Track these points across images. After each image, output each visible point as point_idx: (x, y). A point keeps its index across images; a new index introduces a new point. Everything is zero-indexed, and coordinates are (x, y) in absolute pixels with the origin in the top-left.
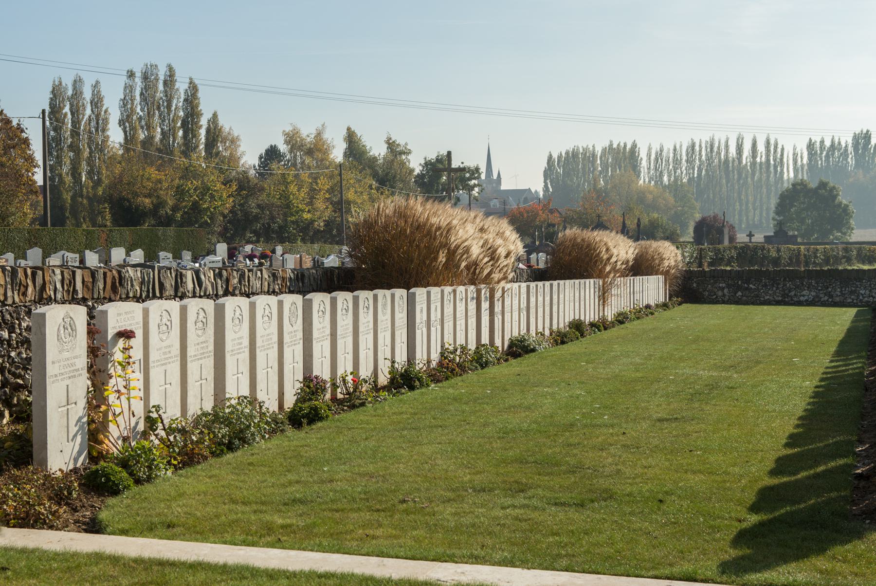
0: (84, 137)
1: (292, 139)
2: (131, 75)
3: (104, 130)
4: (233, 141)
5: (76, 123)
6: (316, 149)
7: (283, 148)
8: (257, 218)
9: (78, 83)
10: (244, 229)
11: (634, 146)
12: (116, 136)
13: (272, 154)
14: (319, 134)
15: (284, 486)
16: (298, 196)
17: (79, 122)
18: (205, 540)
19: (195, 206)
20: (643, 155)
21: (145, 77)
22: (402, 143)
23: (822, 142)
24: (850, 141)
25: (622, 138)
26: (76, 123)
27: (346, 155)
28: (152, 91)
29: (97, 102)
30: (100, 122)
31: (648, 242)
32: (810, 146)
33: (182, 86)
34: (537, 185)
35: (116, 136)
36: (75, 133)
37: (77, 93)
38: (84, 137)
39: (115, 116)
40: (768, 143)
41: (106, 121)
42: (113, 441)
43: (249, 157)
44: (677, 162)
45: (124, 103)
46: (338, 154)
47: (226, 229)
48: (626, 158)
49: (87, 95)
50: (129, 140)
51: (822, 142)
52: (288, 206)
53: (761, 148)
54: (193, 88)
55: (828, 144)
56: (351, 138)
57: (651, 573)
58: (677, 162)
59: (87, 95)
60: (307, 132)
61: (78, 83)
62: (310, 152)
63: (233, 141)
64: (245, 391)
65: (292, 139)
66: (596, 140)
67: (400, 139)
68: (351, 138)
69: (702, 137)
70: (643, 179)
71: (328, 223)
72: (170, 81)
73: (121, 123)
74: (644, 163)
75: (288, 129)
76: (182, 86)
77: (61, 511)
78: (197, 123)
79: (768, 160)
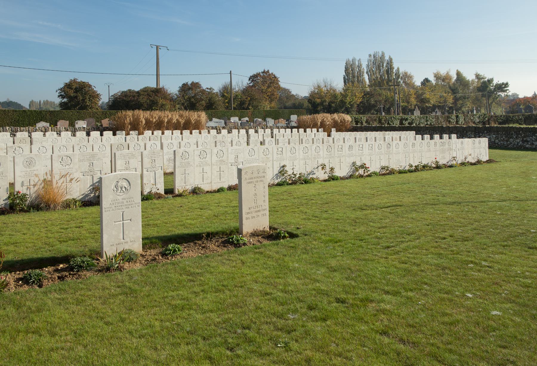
1: (437, 77)
2: (370, 56)
3: (363, 75)
4: (411, 77)
7: (432, 79)
13: (426, 81)
14: (448, 73)
15: (502, 253)
17: (355, 73)
18: (188, 234)
21: (374, 57)
22: (482, 75)
29: (360, 66)
30: (360, 73)
33: (387, 58)
41: (363, 72)
42: (145, 193)
43: (418, 82)
45: (368, 66)
49: (357, 63)
54: (391, 60)
56: (398, 69)
59: (357, 63)
62: (443, 80)
63: (411, 77)
65: (437, 77)
75: (435, 72)
76: (387, 58)
77: (462, 332)
78: (392, 71)
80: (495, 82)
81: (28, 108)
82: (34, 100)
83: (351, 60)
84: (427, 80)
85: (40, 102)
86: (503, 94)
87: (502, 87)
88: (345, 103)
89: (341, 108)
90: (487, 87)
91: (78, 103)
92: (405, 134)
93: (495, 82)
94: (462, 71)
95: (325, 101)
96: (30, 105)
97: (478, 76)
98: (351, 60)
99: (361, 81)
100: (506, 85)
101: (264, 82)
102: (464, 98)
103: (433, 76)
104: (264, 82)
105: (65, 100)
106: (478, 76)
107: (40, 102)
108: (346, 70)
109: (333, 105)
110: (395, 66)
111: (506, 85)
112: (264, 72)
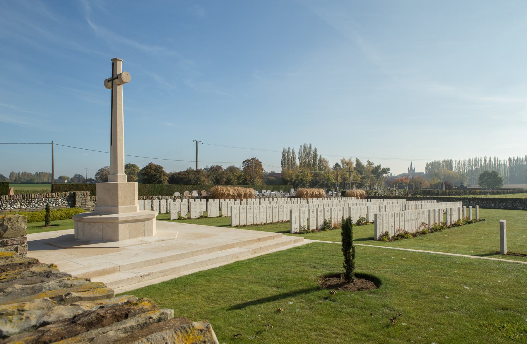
0: (290, 162)
1: (343, 162)
2: (301, 146)
5: (288, 159)
6: (349, 163)
7: (340, 163)
8: (319, 182)
9: (289, 149)
10: (316, 185)
11: (451, 160)
12: (298, 162)
13: (337, 165)
14: (350, 160)
16: (332, 177)
19: (301, 179)
20: (454, 163)
21: (304, 147)
23: (514, 158)
24: (524, 158)
25: (448, 158)
26: (288, 159)
27: (356, 165)
28: (306, 151)
29: (293, 153)
30: (294, 158)
31: (216, 187)
32: (510, 159)
33: (313, 149)
34: (423, 171)
35: (298, 162)
36: (288, 160)
37: (289, 152)
38: (290, 162)
39: (297, 156)
40: (495, 159)
41: (295, 158)
43: (331, 166)
44: (465, 165)
45: (299, 153)
46: (354, 165)
47: (310, 185)
48: (449, 164)
49: (291, 151)
50: (301, 163)
51: (514, 158)
52: (329, 179)
53: (492, 160)
54: (316, 149)
55: (516, 158)
56: (357, 161)
57: (216, 224)
58: (465, 165)
59: (291, 151)
60: (347, 159)
61: (289, 149)
64: (154, 201)
65: (343, 162)
66: (441, 158)
67: (371, 161)
68: (357, 161)
69: (473, 157)
70: (454, 169)
71: (341, 183)
72: (310, 148)
73: (299, 158)
74: (454, 165)
75: (342, 158)
76: (313, 149)
79: (495, 164)
80: (382, 168)
81: (9, 178)
82: (14, 172)
83: (287, 149)
84: (337, 165)
85: (19, 173)
86: (384, 175)
87: (386, 171)
88: (304, 181)
89: (301, 183)
90: (378, 170)
91: (157, 179)
92: (426, 203)
93: (382, 168)
94: (359, 159)
95: (292, 179)
96: (10, 176)
97: (370, 163)
98: (287, 149)
99: (294, 164)
100: (388, 169)
101: (253, 165)
102: (367, 177)
103: (340, 161)
104: (253, 165)
105: (146, 177)
106: (370, 163)
107: (19, 173)
108: (284, 155)
109: (297, 182)
110: (319, 154)
111: (388, 169)
112: (253, 159)
